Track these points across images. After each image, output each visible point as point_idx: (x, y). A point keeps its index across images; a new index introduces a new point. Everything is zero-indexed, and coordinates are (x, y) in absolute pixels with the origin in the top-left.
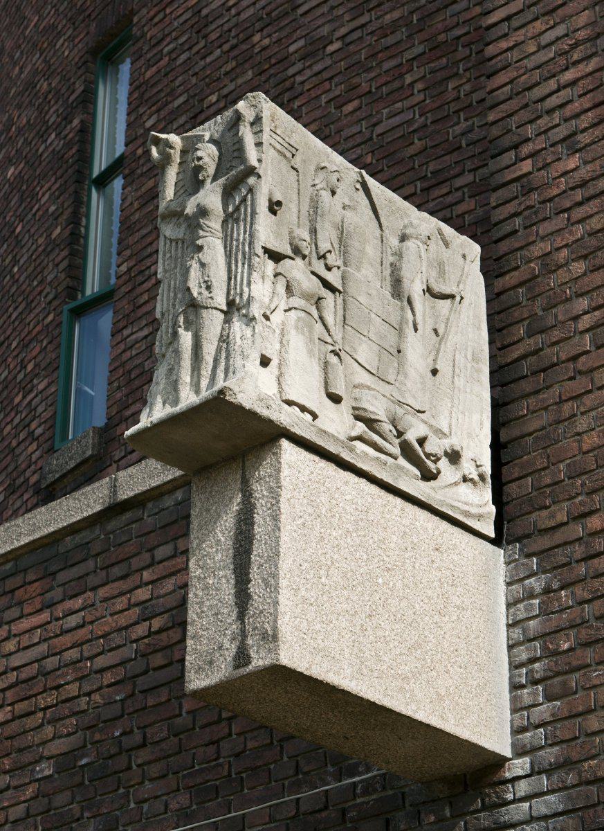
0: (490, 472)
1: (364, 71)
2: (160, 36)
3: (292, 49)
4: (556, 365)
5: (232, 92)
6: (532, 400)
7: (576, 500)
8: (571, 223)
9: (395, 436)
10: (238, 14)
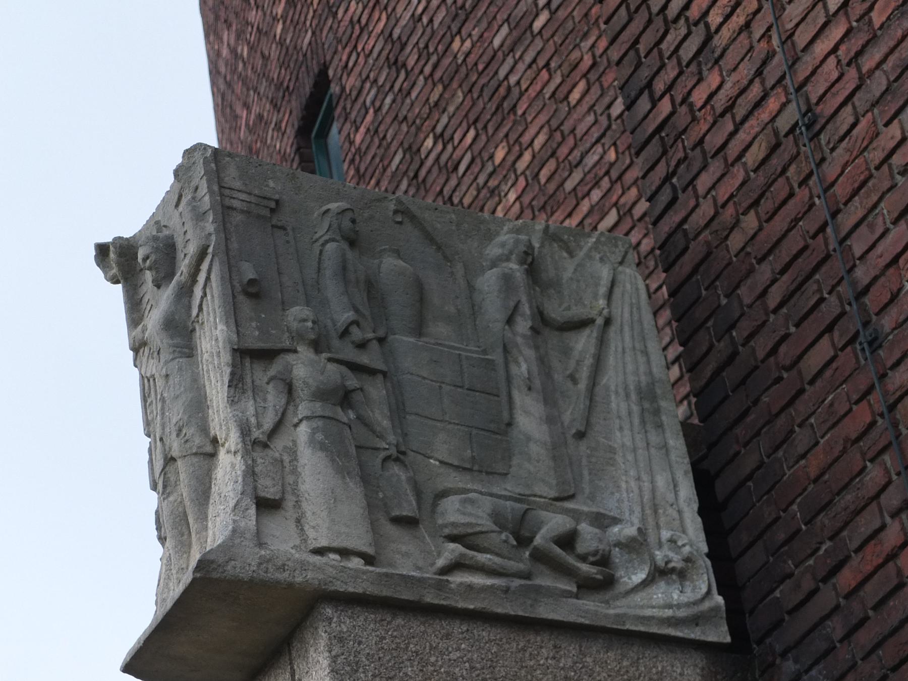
0: (705, 549)
1: (581, 40)
2: (358, 84)
3: (497, 42)
4: (756, 368)
5: (446, 126)
6: (739, 431)
7: (821, 552)
8: (729, 166)
9: (513, 546)
10: (431, 21)
